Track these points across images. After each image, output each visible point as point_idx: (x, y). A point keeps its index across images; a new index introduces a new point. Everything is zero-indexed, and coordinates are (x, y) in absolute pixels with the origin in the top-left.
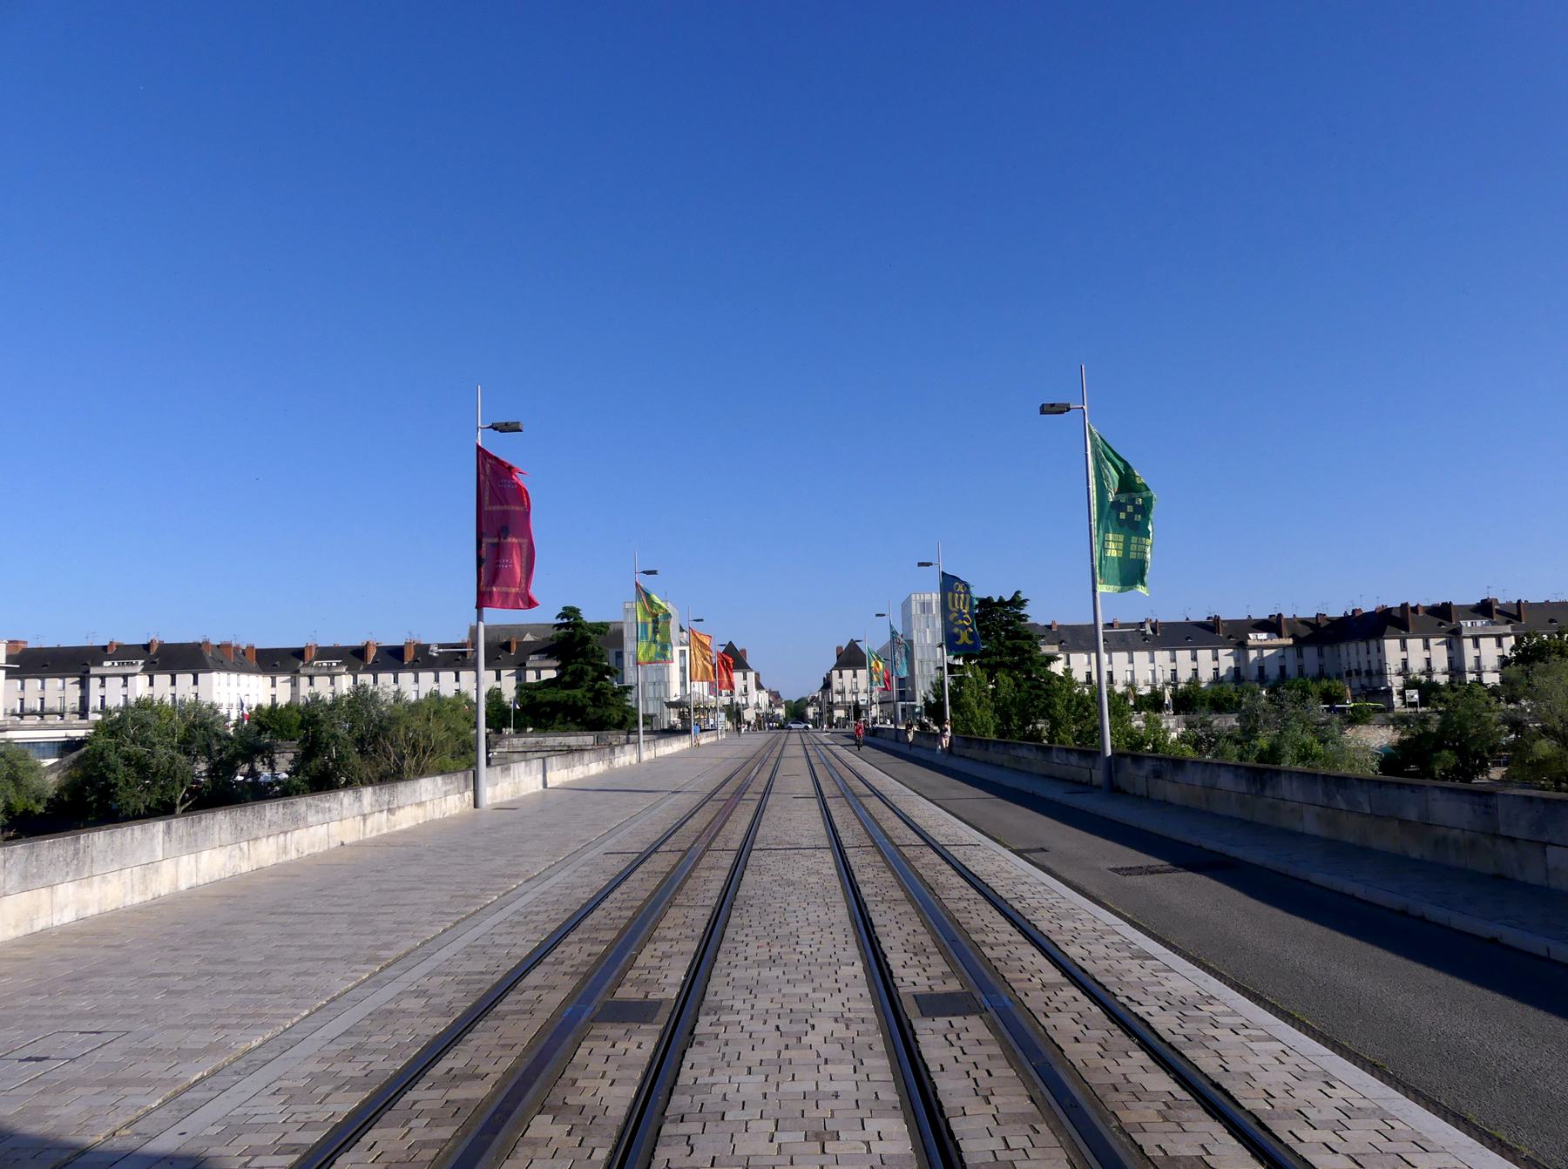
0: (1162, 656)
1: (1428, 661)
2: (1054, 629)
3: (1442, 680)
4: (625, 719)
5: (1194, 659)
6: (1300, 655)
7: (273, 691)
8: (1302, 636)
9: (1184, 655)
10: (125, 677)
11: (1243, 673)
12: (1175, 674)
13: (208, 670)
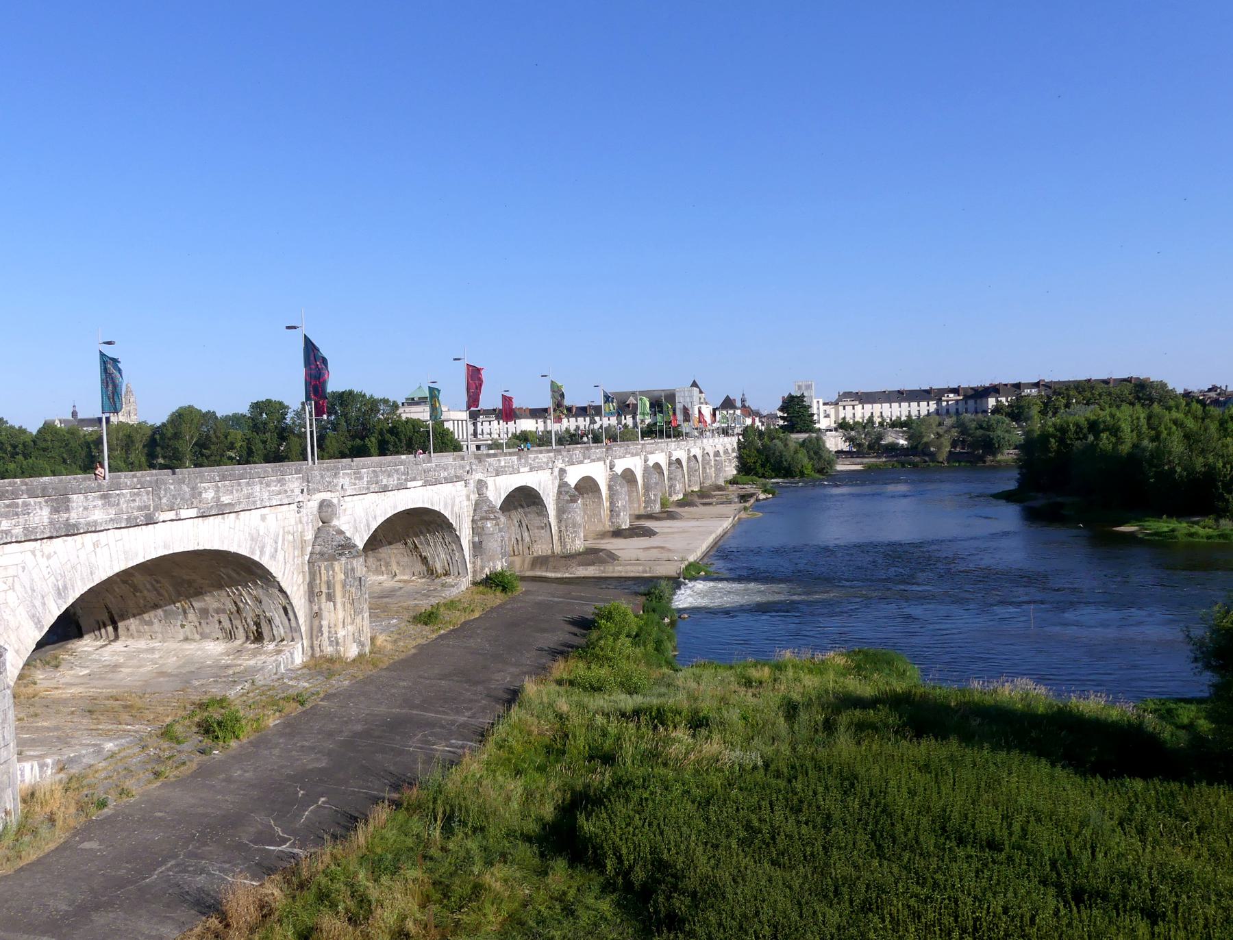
0: (905, 405)
1: (854, 414)
5: (919, 406)
6: (966, 403)
9: (914, 404)
10: (490, 422)
13: (519, 418)
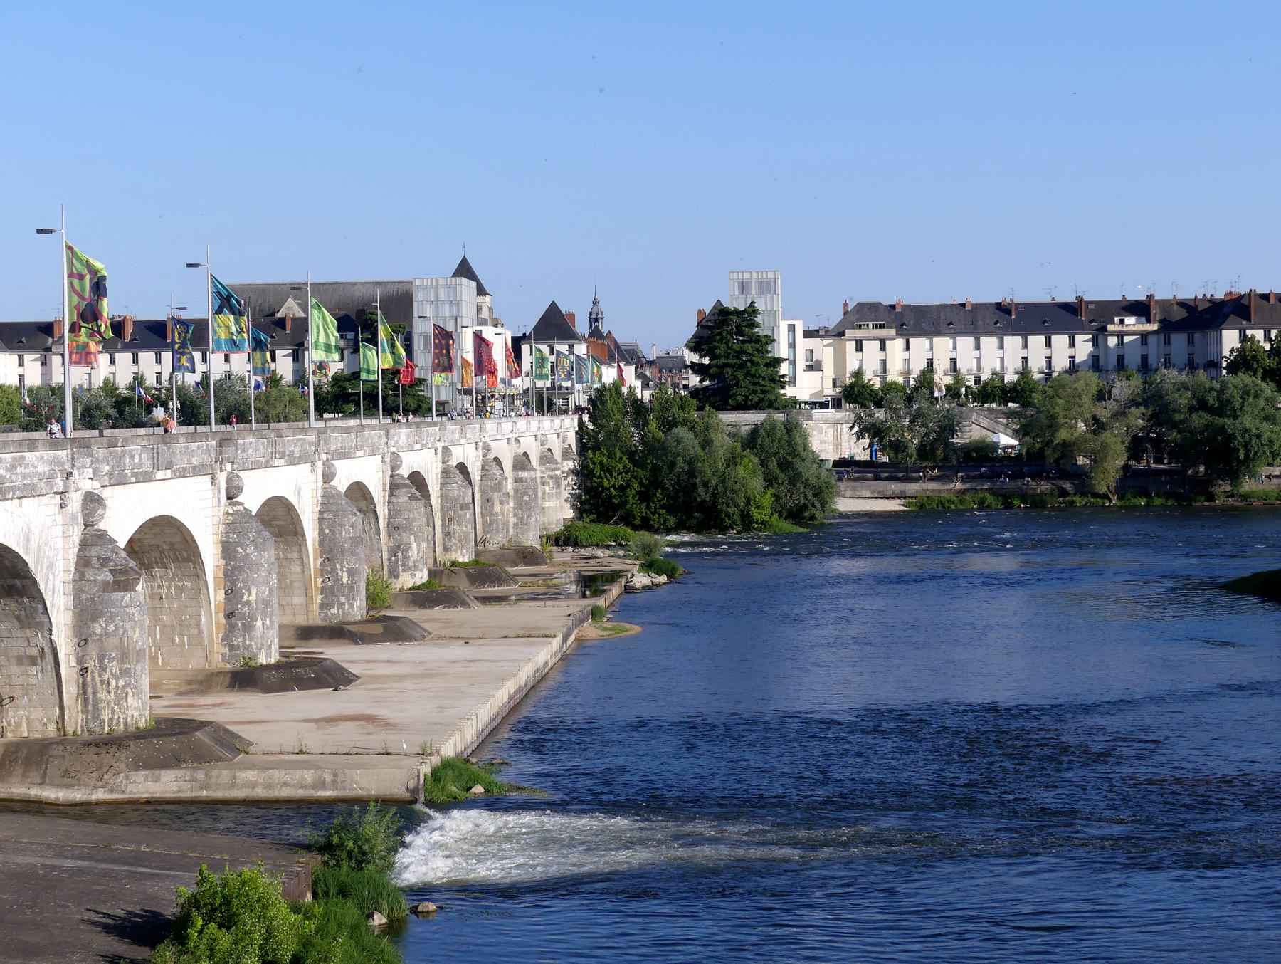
2: (898, 310)
3: (80, 733)
4: (419, 406)
6: (1167, 342)
7: (21, 371)
8: (1173, 320)
9: (1037, 341)
11: (1101, 362)
12: (1050, 362)
